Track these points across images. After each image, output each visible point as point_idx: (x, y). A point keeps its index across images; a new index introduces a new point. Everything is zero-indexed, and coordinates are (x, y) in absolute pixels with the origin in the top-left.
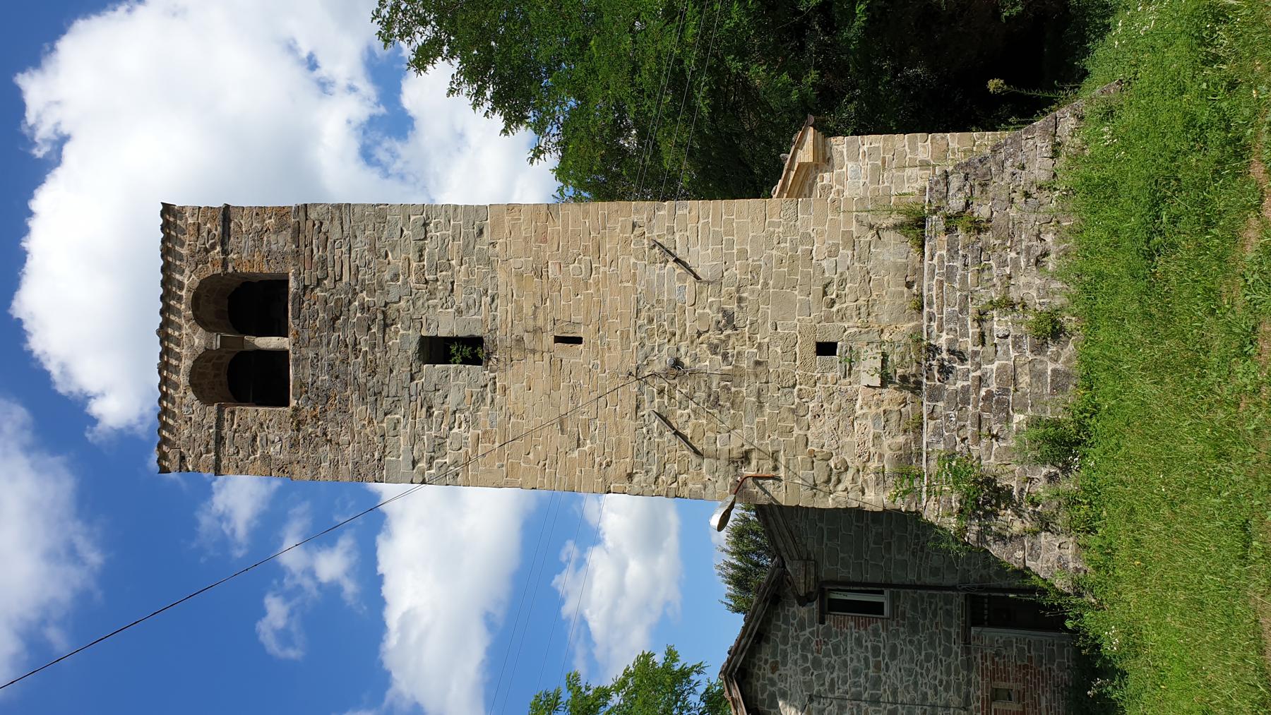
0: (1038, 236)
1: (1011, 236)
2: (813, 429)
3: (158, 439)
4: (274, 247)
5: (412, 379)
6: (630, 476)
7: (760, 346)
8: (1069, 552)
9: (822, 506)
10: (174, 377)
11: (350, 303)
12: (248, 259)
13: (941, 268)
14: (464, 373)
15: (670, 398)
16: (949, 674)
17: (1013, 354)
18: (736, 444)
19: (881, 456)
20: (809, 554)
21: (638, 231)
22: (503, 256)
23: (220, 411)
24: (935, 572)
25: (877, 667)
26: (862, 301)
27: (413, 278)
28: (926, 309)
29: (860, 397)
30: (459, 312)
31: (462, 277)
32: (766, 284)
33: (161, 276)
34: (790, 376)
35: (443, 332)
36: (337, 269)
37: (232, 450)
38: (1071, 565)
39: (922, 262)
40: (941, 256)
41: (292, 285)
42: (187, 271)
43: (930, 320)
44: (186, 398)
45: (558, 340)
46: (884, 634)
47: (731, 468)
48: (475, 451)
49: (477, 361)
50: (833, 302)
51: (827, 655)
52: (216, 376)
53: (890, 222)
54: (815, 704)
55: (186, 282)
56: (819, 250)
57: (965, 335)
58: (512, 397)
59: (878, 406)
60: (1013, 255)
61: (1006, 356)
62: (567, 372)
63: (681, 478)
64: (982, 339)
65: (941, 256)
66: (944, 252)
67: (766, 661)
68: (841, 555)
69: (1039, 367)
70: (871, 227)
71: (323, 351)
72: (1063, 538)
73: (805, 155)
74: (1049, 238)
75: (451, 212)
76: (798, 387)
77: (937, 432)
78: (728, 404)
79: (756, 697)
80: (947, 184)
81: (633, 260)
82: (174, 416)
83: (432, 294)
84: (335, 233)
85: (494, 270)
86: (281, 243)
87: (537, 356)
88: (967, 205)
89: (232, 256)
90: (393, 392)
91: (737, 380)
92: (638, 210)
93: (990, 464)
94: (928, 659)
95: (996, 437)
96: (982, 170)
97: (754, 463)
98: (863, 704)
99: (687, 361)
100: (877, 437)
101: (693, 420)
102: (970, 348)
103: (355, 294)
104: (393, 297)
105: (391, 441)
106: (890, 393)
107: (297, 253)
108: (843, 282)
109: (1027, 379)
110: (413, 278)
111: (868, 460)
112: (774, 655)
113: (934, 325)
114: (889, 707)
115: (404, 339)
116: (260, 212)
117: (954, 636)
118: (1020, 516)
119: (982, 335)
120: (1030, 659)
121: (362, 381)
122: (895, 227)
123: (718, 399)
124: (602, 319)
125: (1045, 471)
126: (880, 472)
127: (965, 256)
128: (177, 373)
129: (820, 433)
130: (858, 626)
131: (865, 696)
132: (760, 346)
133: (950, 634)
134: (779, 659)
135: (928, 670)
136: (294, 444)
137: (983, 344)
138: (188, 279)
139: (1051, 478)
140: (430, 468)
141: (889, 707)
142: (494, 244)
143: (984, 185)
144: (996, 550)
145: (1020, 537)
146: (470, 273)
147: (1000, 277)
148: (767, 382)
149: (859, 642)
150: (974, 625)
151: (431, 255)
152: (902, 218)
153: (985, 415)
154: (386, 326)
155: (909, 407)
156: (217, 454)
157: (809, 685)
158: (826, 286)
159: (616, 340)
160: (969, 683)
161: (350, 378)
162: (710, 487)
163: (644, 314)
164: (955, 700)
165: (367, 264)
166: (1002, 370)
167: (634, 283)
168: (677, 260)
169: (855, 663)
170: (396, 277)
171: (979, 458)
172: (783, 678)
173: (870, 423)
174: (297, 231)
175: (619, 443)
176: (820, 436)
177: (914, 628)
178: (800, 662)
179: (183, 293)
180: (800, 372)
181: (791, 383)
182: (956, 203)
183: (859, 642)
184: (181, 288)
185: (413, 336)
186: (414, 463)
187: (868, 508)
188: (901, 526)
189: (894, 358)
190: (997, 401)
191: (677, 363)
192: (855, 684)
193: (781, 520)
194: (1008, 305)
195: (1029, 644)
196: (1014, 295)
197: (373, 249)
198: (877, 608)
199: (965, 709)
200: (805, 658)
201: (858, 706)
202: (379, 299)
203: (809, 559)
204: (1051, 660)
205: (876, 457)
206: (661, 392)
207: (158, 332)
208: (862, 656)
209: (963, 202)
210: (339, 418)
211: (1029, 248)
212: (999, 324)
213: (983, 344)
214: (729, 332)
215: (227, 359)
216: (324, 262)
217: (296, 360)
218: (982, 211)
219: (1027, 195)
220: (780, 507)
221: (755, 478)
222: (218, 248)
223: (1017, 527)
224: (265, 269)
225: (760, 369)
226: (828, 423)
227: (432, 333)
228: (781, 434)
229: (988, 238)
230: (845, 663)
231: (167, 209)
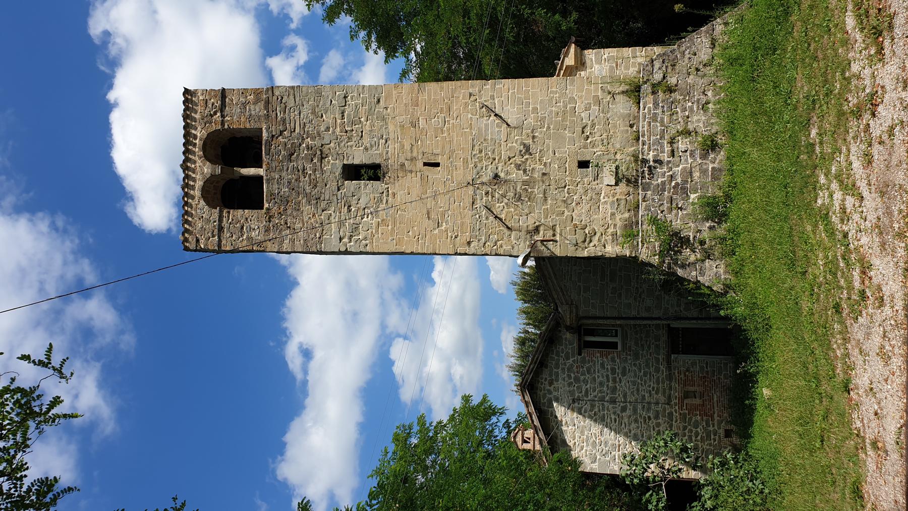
0: (703, 93)
1: (689, 94)
2: (576, 211)
3: (183, 229)
4: (253, 113)
5: (339, 190)
6: (469, 243)
7: (545, 164)
8: (721, 271)
9: (581, 256)
10: (192, 192)
11: (300, 145)
12: (236, 120)
13: (649, 114)
14: (370, 186)
15: (493, 197)
16: (658, 384)
17: (690, 161)
18: (531, 223)
19: (615, 225)
20: (572, 301)
21: (473, 98)
22: (392, 115)
23: (221, 212)
24: (648, 309)
25: (614, 380)
26: (604, 136)
27: (338, 129)
28: (641, 139)
30: (366, 149)
31: (368, 128)
32: (549, 128)
33: (183, 132)
35: (357, 162)
36: (292, 125)
37: (228, 235)
38: (723, 277)
39: (638, 112)
40: (649, 108)
41: (265, 135)
42: (199, 128)
43: (644, 144)
44: (199, 205)
45: (425, 164)
47: (528, 236)
48: (377, 231)
49: (377, 178)
50: (588, 137)
52: (215, 194)
53: (621, 89)
54: (576, 404)
55: (199, 135)
56: (580, 107)
57: (663, 152)
58: (399, 199)
59: (613, 196)
60: (690, 104)
61: (687, 162)
62: (431, 183)
63: (499, 243)
64: (673, 153)
65: (649, 108)
66: (651, 105)
67: (546, 379)
69: (705, 167)
70: (610, 93)
71: (284, 174)
72: (718, 262)
73: (570, 61)
74: (710, 94)
75: (360, 90)
77: (648, 209)
80: (653, 66)
81: (470, 116)
82: (192, 215)
83: (350, 139)
84: (291, 103)
85: (386, 124)
86: (258, 110)
87: (413, 174)
88: (664, 77)
89: (227, 118)
90: (327, 198)
91: (532, 184)
92: (475, 85)
93: (677, 224)
94: (645, 375)
95: (681, 209)
96: (672, 57)
97: (541, 232)
99: (502, 175)
100: (613, 214)
101: (506, 209)
102: (666, 159)
103: (303, 139)
104: (326, 141)
105: (326, 227)
106: (623, 187)
107: (267, 116)
108: (593, 125)
109: (698, 174)
110: (338, 129)
112: (551, 375)
113: (646, 147)
114: (622, 404)
115: (333, 166)
116: (244, 92)
117: (661, 360)
118: (694, 252)
119: (673, 151)
120: (707, 372)
121: (308, 191)
122: (623, 92)
123: (520, 196)
124: (452, 152)
125: (708, 225)
126: (614, 235)
127: (663, 107)
128: (194, 190)
129: (580, 214)
130: (602, 356)
131: (607, 398)
132: (545, 164)
135: (645, 382)
136: (267, 230)
137: (673, 156)
138: (200, 133)
139: (711, 228)
140: (350, 242)
141: (622, 404)
142: (386, 108)
143: (673, 65)
144: (680, 272)
145: (694, 264)
146: (372, 125)
147: (683, 117)
149: (602, 365)
151: (349, 115)
152: (627, 87)
153: (674, 197)
154: (322, 158)
155: (631, 197)
156: (219, 237)
157: (572, 393)
158: (584, 128)
159: (460, 164)
161: (301, 190)
162: (516, 248)
163: (477, 148)
164: (662, 399)
165: (310, 122)
166: (684, 169)
167: (471, 129)
168: (496, 115)
169: (601, 379)
170: (328, 129)
171: (671, 221)
172: (556, 389)
173: (609, 207)
174: (267, 102)
175: (462, 224)
177: (636, 356)
179: (197, 141)
180: (569, 178)
182: (658, 77)
183: (602, 365)
184: (196, 139)
185: (339, 164)
186: (341, 239)
187: (607, 255)
188: (628, 267)
189: (623, 168)
191: (496, 176)
192: (600, 391)
194: (687, 133)
195: (707, 363)
196: (691, 127)
197: (314, 113)
198: (614, 346)
199: (668, 404)
202: (317, 142)
203: (572, 304)
206: (487, 193)
207: (182, 166)
209: (662, 75)
210: (295, 214)
211: (698, 100)
212: (682, 144)
213: (673, 156)
215: (222, 183)
216: (284, 120)
217: (268, 180)
218: (672, 81)
219: (697, 70)
220: (557, 257)
221: (542, 241)
222: (219, 114)
223: (692, 258)
224: (248, 126)
225: (545, 177)
226: (585, 207)
227: (350, 162)
228: (557, 215)
229: (677, 96)
231: (186, 92)
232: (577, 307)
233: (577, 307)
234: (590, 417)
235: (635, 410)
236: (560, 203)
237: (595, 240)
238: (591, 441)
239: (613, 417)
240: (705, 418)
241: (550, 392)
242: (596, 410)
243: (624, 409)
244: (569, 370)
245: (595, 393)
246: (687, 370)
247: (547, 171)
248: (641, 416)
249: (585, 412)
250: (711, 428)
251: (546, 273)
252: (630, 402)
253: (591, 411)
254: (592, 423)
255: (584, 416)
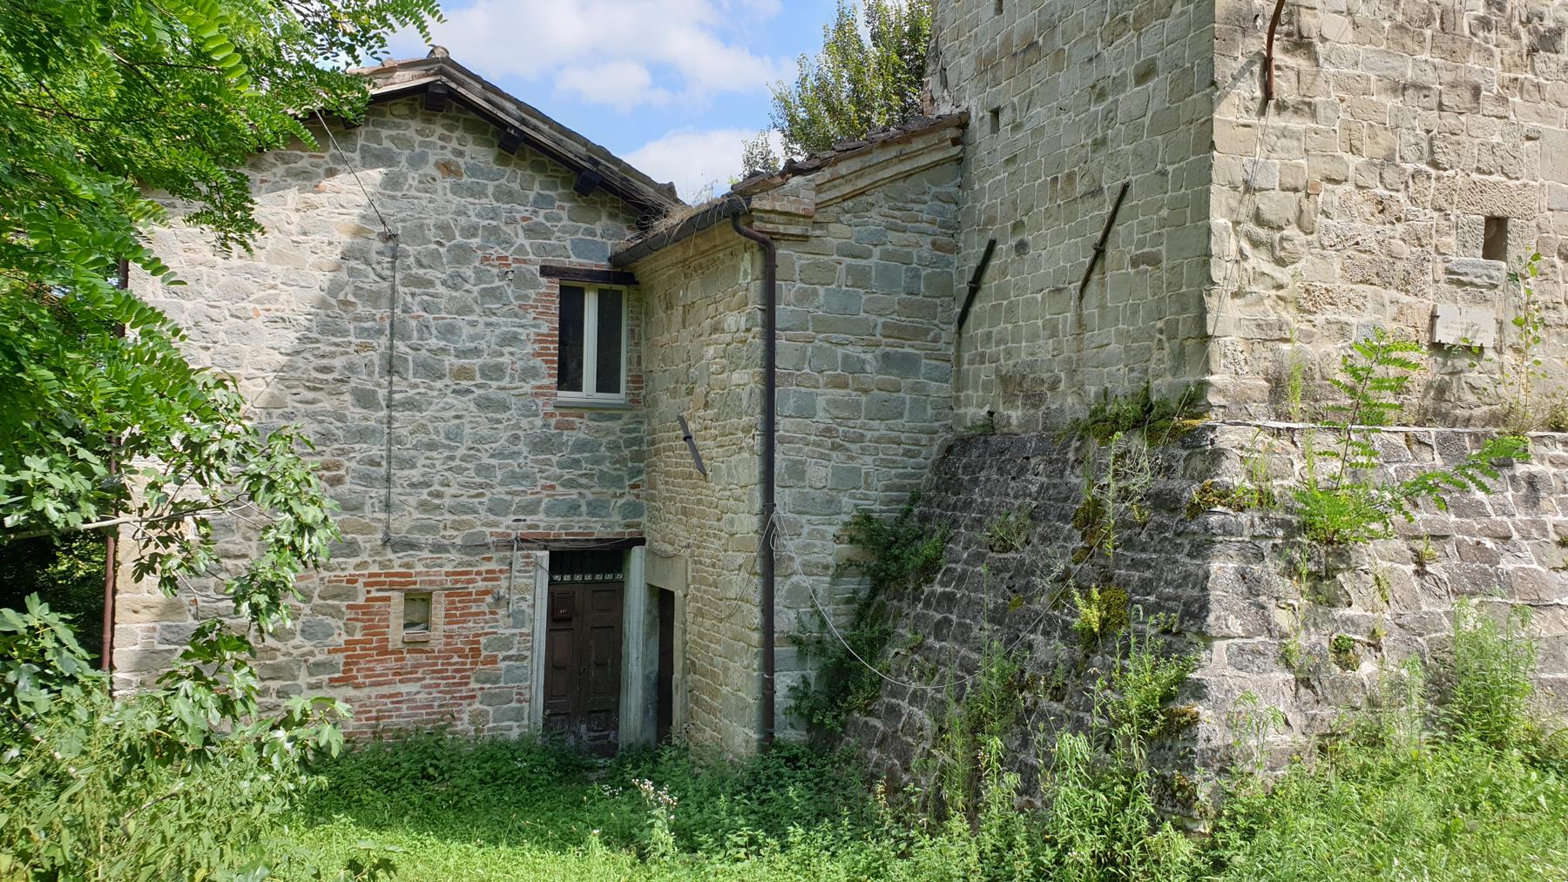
2: (1357, 197)
24: (797, 471)
25: (463, 373)
29: (1411, 299)
34: (1454, 158)
46: (527, 388)
51: (480, 276)
54: (378, 245)
68: (821, 290)
72: (1297, 720)
76: (1433, 172)
78: (1400, 18)
79: (383, 125)
94: (481, 469)
98: (384, 341)
100: (1343, 330)
111: (1300, 309)
112: (473, 171)
114: (382, 393)
133: (534, 512)
134: (466, 179)
135: (460, 470)
141: (382, 393)
145: (1268, 628)
148: (1441, 107)
149: (511, 339)
150: (552, 554)
157: (418, 233)
160: (438, 548)
172: (427, 184)
176: (1344, 208)
178: (463, 220)
180: (1460, 180)
181: (1441, 158)
183: (511, 339)
190: (1485, 573)
193: (887, 173)
199: (385, 542)
200: (471, 231)
201: (380, 332)
204: (489, 699)
205: (1305, 326)
208: (483, 345)
214: (1525, 39)
225: (1467, 96)
226: (1367, 231)
230: (464, 310)
232: (804, 238)
233: (804, 238)
234: (335, 288)
235: (362, 435)
236: (1385, 138)
237: (1259, 261)
238: (253, 287)
239: (338, 362)
240: (340, 658)
241: (417, 161)
242: (361, 309)
243: (365, 399)
244: (494, 231)
245: (417, 310)
246: (498, 599)
247: (1488, 106)
248: (343, 452)
249: (352, 272)
250: (304, 679)
251: (918, 144)
252: (390, 420)
253: (358, 291)
254: (315, 292)
255: (337, 268)
